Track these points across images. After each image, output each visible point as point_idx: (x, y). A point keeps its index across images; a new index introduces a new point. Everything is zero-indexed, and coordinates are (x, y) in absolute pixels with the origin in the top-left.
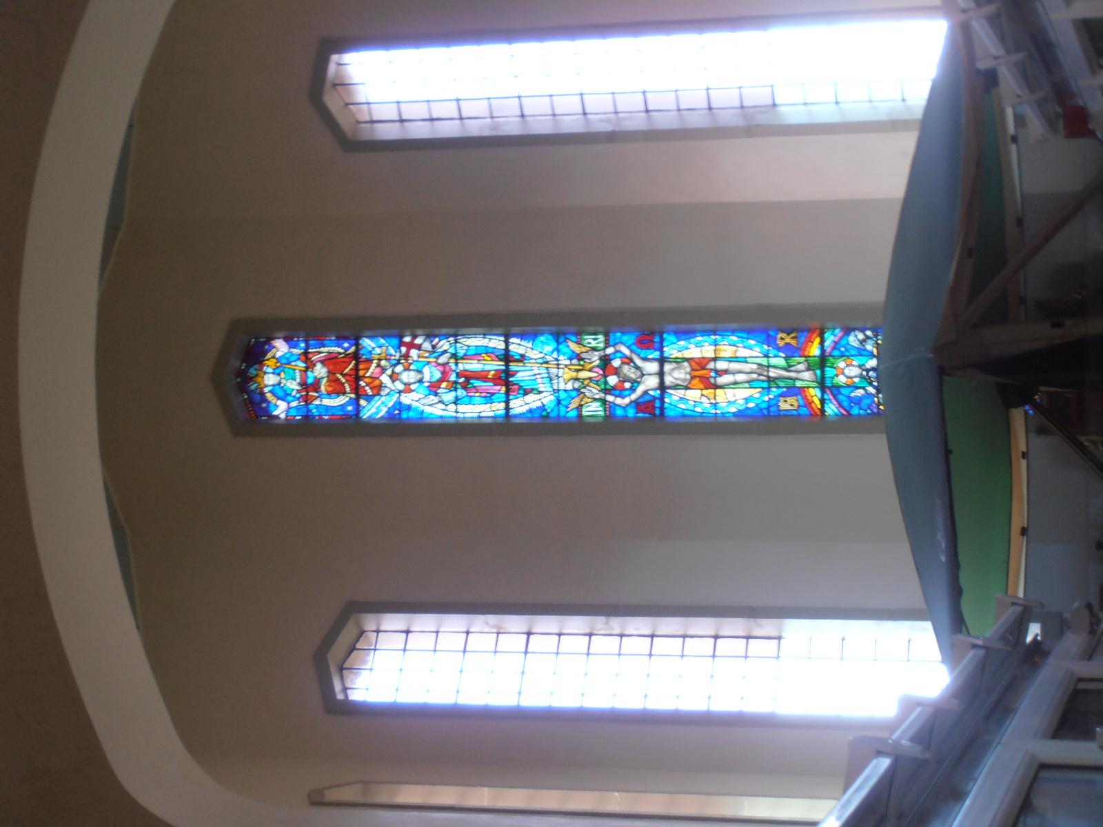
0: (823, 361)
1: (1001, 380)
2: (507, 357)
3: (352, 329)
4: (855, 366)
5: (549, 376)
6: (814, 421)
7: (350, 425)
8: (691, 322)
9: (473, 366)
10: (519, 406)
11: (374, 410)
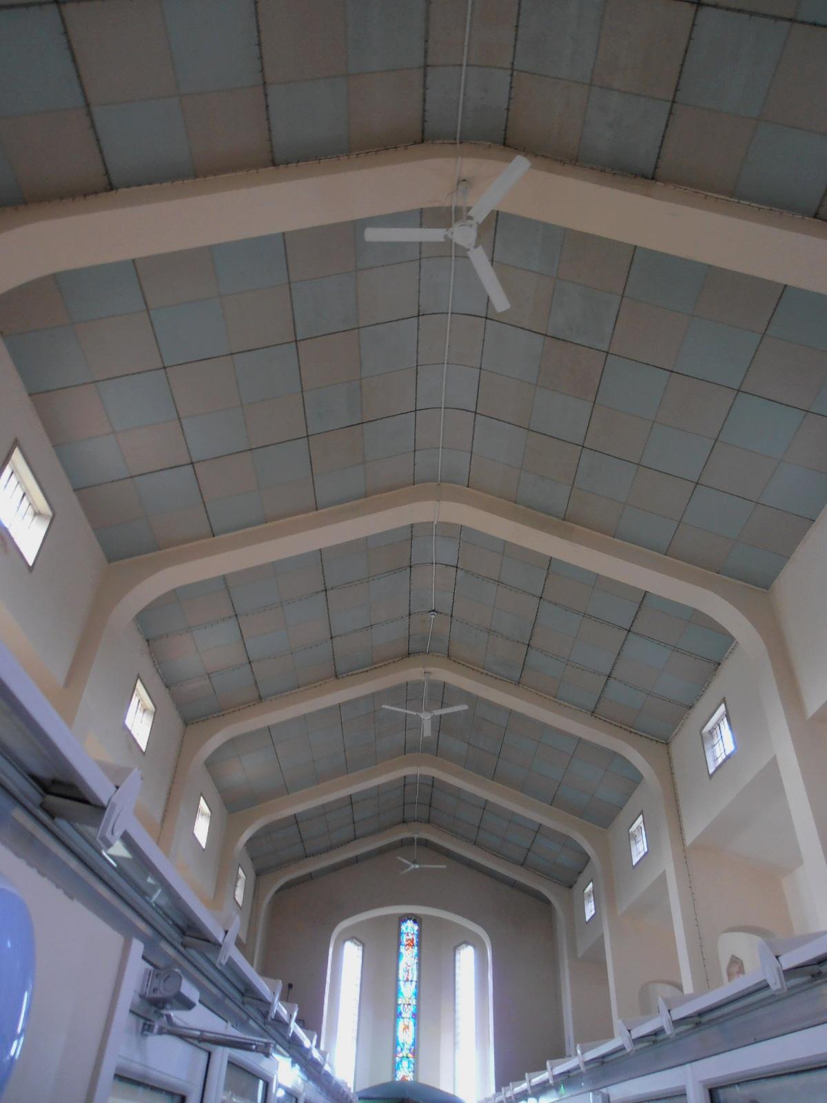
0: (407, 1057)
1: (409, 870)
2: (412, 981)
3: (419, 945)
4: (405, 1072)
5: (407, 991)
6: (395, 1054)
7: (399, 943)
8: (417, 1025)
9: (410, 974)
10: (401, 983)
11: (402, 949)
